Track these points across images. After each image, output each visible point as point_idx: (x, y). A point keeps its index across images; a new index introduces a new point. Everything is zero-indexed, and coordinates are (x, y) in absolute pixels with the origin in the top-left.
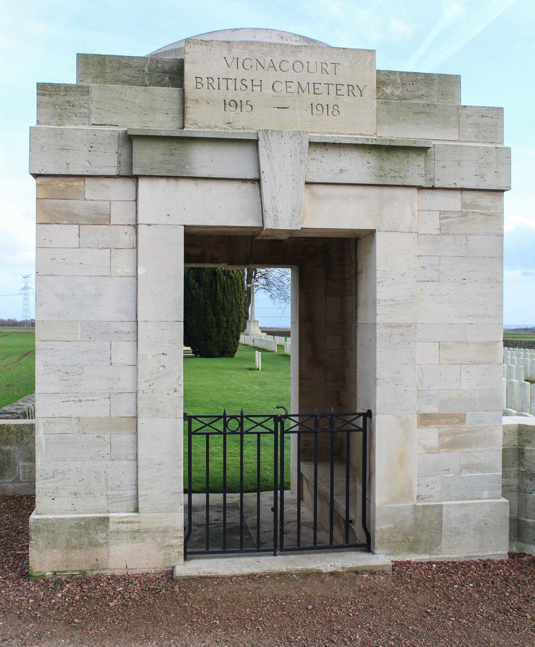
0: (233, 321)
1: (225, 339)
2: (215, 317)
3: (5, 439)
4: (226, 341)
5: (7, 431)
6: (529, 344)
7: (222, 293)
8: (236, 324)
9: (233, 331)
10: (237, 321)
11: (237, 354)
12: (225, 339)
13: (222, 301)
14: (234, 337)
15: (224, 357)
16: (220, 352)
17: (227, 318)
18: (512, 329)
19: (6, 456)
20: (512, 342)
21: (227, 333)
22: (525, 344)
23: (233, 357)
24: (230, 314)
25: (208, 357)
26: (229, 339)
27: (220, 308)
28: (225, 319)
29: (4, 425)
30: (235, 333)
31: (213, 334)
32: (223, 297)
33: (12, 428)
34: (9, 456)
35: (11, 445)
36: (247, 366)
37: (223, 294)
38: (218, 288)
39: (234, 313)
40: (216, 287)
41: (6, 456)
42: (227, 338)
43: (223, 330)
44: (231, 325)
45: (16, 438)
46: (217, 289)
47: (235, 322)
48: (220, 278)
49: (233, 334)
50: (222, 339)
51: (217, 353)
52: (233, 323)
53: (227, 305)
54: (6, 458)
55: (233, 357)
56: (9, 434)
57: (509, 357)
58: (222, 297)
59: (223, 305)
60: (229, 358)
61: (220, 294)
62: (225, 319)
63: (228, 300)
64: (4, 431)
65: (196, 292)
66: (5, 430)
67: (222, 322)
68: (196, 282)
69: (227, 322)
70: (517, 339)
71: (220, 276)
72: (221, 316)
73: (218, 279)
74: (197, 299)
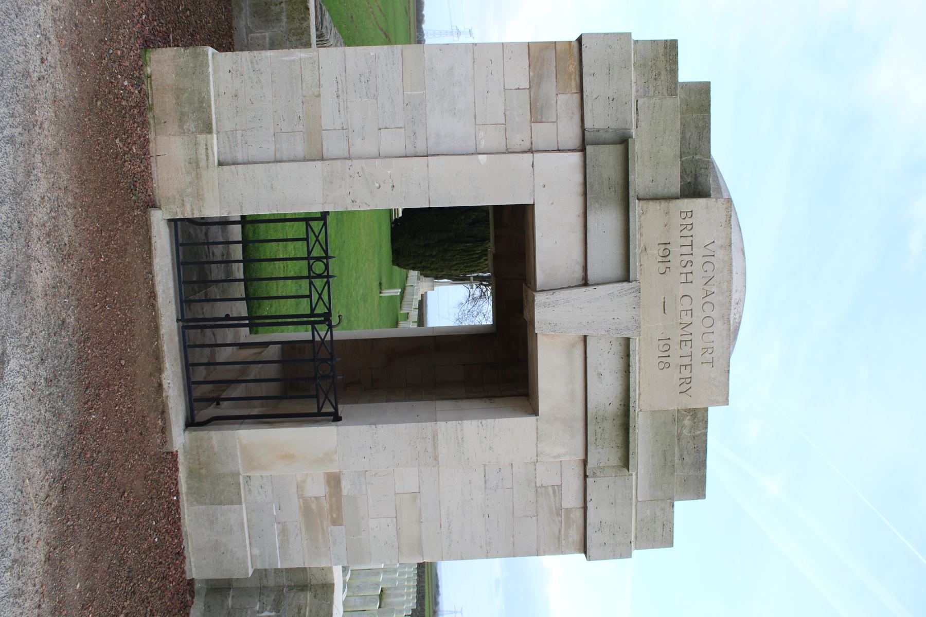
1: (413, 255)
5: (302, 18)
7: (463, 249)
8: (429, 265)
9: (421, 263)
10: (432, 267)
11: (396, 268)
12: (413, 255)
20: (423, 572)
28: (434, 253)
30: (419, 266)
32: (459, 250)
33: (306, 23)
34: (276, 21)
35: (288, 23)
36: (384, 281)
37: (461, 250)
38: (468, 244)
40: (468, 242)
45: (295, 27)
52: (430, 262)
54: (273, 18)
60: (391, 260)
62: (434, 253)
63: (454, 256)
64: (302, 14)
65: (462, 220)
66: (303, 16)
69: (431, 256)
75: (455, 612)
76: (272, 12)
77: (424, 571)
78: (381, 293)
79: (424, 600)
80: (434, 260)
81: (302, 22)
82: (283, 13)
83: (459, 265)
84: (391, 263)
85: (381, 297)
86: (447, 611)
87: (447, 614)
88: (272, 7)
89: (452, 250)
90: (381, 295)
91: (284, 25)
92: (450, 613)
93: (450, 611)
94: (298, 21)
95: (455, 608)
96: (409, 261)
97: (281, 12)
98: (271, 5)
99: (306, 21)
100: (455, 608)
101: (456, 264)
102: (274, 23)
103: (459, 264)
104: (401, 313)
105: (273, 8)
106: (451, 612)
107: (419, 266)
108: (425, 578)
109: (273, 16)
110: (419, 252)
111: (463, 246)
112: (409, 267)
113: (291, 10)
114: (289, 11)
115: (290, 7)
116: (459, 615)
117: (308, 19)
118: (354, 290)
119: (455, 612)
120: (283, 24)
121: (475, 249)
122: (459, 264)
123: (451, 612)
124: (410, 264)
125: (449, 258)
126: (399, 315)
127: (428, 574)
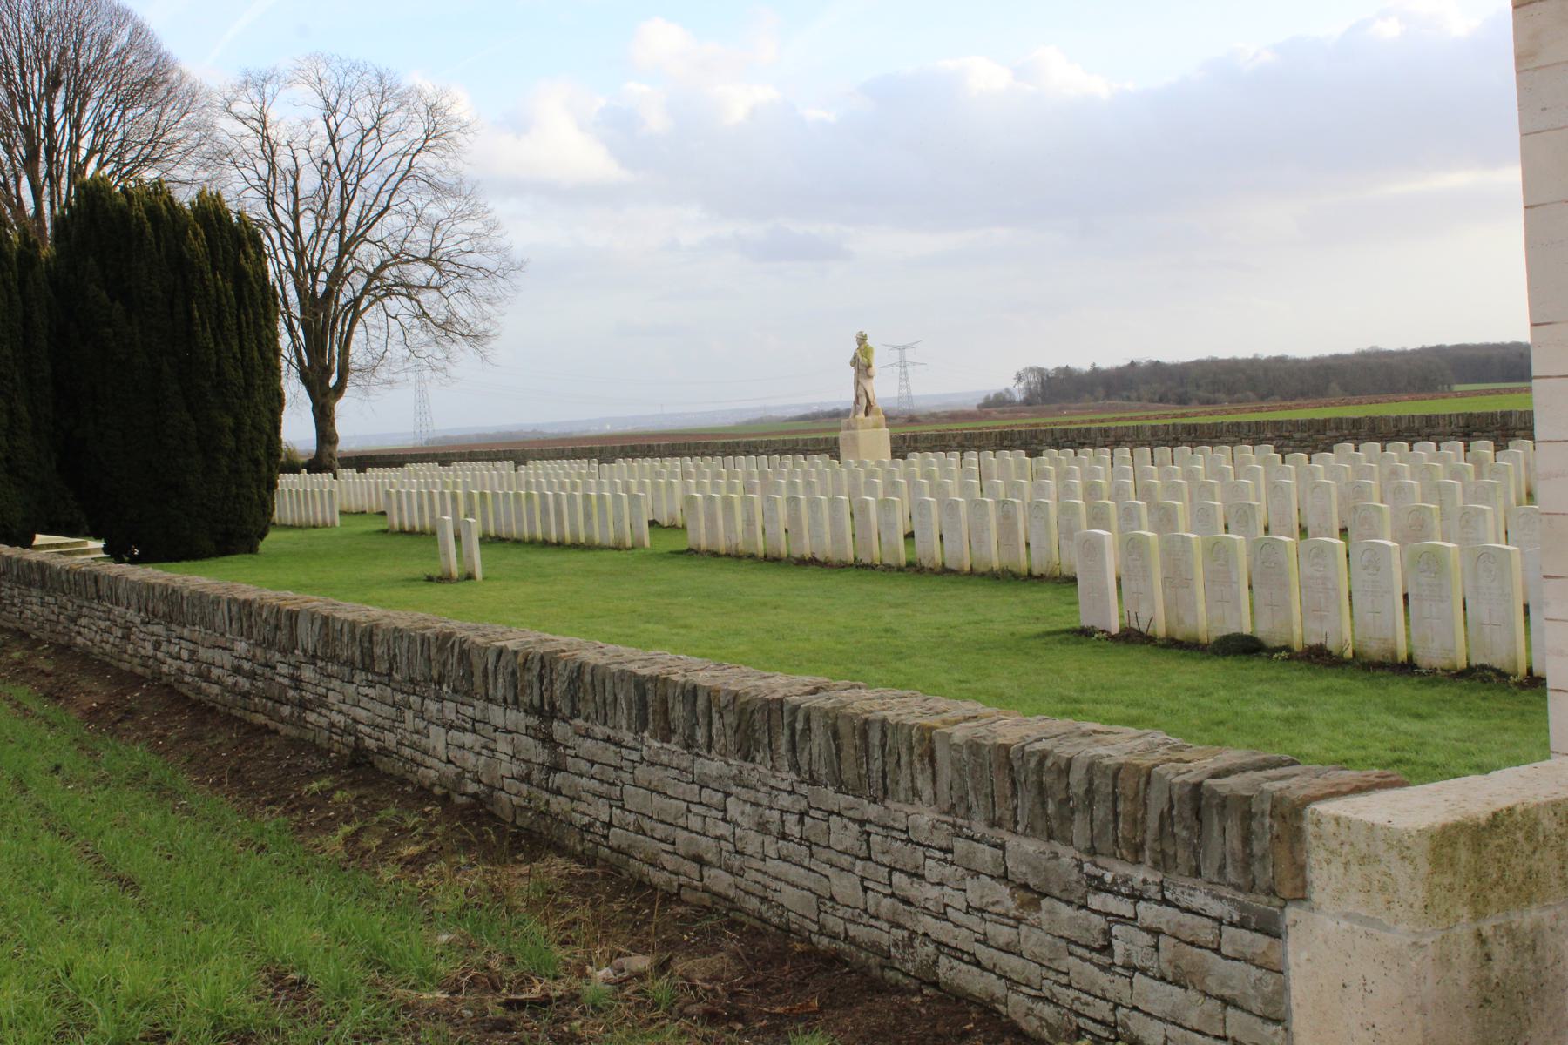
0: (254, 426)
1: (234, 489)
3: (1520, 878)
5: (1528, 838)
6: (1167, 433)
7: (212, 329)
8: (265, 437)
9: (256, 462)
11: (263, 546)
12: (234, 489)
13: (214, 359)
15: (234, 553)
19: (1527, 956)
20: (1106, 432)
22: (1153, 435)
24: (245, 402)
28: (229, 421)
29: (1510, 810)
30: (264, 469)
32: (217, 344)
33: (1545, 822)
35: (1544, 900)
36: (420, 568)
37: (215, 336)
38: (196, 314)
40: (189, 312)
44: (251, 440)
45: (1557, 863)
46: (190, 318)
47: (261, 431)
49: (258, 472)
52: (255, 433)
54: (1529, 966)
57: (1080, 502)
58: (212, 345)
60: (248, 556)
62: (229, 421)
64: (1516, 842)
66: (1520, 835)
69: (237, 430)
70: (1120, 424)
71: (202, 272)
75: (903, 364)
76: (1512, 973)
77: (1100, 429)
78: (470, 577)
79: (1202, 426)
80: (249, 421)
81: (1541, 838)
82: (1514, 926)
83: (264, 342)
84: (254, 556)
85: (485, 579)
86: (901, 387)
87: (908, 387)
88: (1493, 976)
89: (218, 365)
90: (479, 574)
91: (1551, 912)
92: (907, 380)
94: (1537, 856)
95: (892, 365)
97: (1511, 933)
98: (1488, 980)
99: (1536, 822)
100: (892, 365)
101: (259, 349)
102: (1543, 959)
103: (259, 342)
105: (1497, 971)
106: (904, 376)
108: (1128, 428)
109: (1522, 969)
110: (226, 471)
111: (204, 329)
113: (1501, 889)
115: (1493, 896)
116: (910, 356)
117: (1526, 812)
118: (697, 647)
119: (903, 364)
120: (1547, 915)
121: (212, 292)
123: (904, 376)
127: (1119, 419)
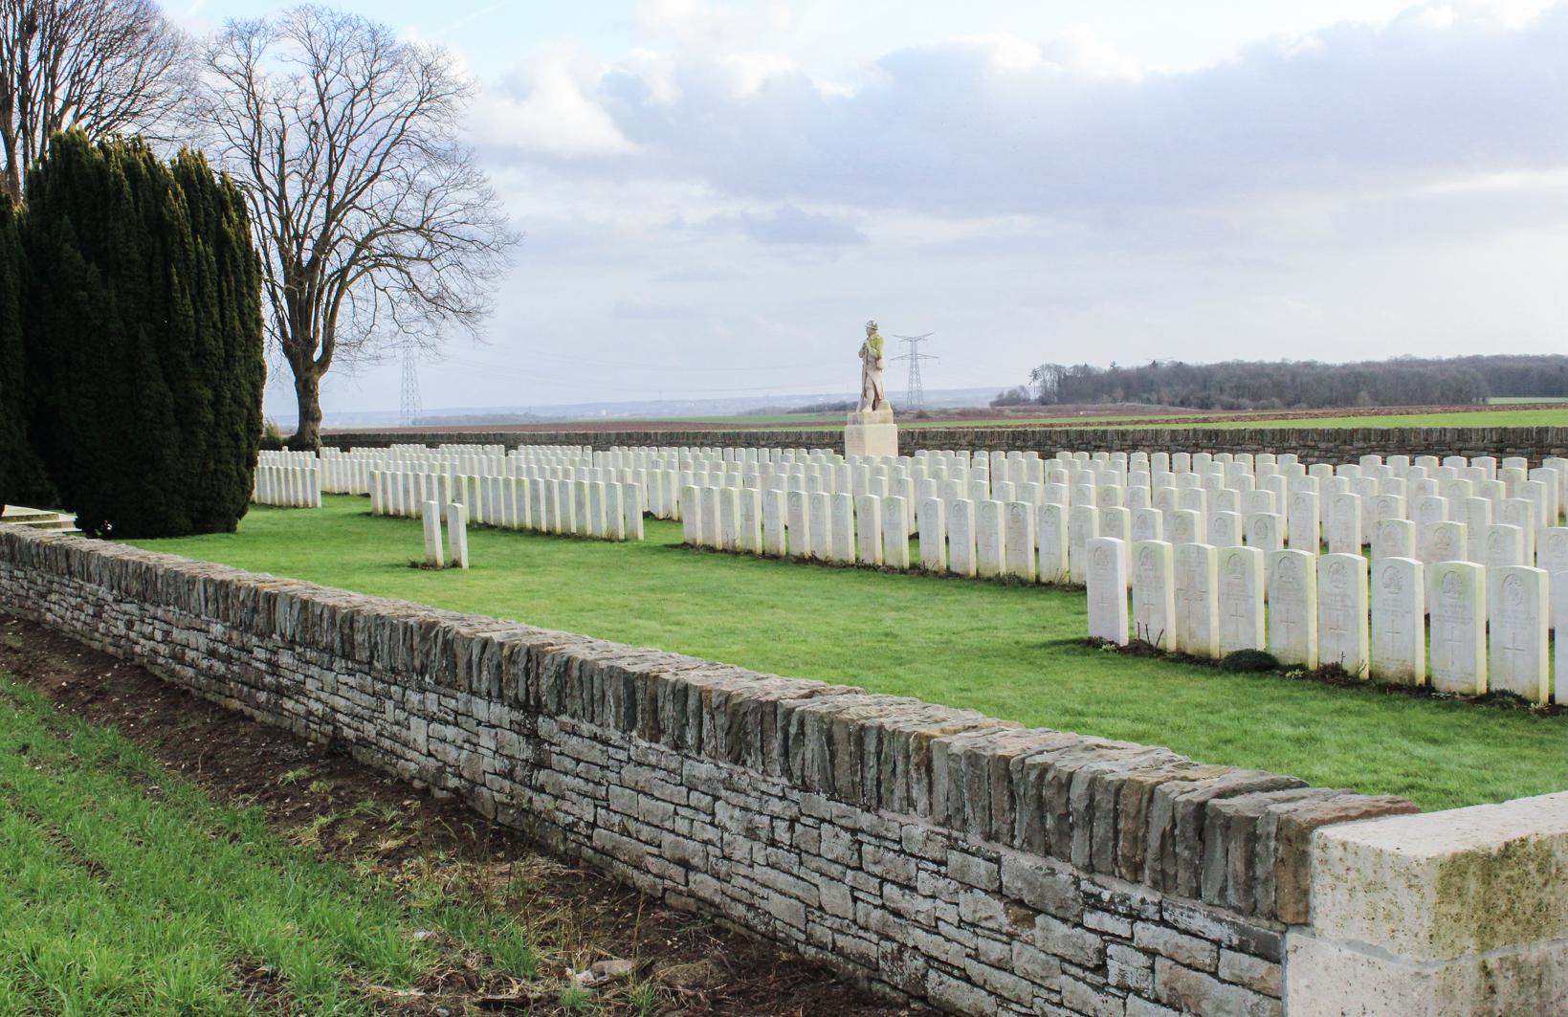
0: (234, 399)
2: (172, 390)
4: (215, 472)
5: (1541, 870)
7: (192, 296)
9: (236, 437)
10: (248, 400)
12: (212, 465)
14: (239, 457)
16: (195, 514)
17: (215, 389)
18: (792, 407)
20: (1123, 435)
21: (216, 446)
23: (230, 528)
24: (225, 374)
25: (153, 537)
26: (222, 467)
27: (187, 354)
29: (1524, 841)
30: (244, 445)
31: (166, 452)
32: (197, 311)
33: (1559, 854)
34: (1545, 986)
35: (1553, 933)
37: (194, 303)
38: (176, 279)
39: (238, 371)
40: (168, 277)
41: (1533, 991)
42: (218, 461)
43: (202, 435)
44: (230, 414)
46: (169, 284)
47: (241, 405)
48: (182, 241)
49: (238, 447)
50: (199, 470)
51: (185, 522)
52: (235, 408)
53: (213, 343)
54: (1535, 1000)
55: (230, 528)
56: (1545, 884)
58: (191, 313)
59: (199, 342)
60: (225, 535)
61: (186, 304)
63: (214, 326)
64: (1527, 874)
65: (91, 298)
66: (1532, 867)
67: (199, 403)
68: (88, 261)
69: (216, 403)
71: (182, 235)
72: (194, 384)
73: (176, 247)
74: (98, 322)
75: (914, 356)
79: (1224, 432)
80: (229, 395)
81: (1554, 871)
87: (918, 381)
90: (465, 563)
93: (912, 373)
94: (1549, 888)
96: (228, 476)
99: (1550, 854)
102: (1548, 993)
103: (241, 313)
104: (323, 506)
107: (244, 445)
109: (1526, 1003)
110: (204, 446)
111: (184, 296)
112: (248, 475)
114: (1514, 928)
121: (193, 256)
122: (241, 313)
124: (239, 474)
125: (221, 343)
126: (328, 511)
